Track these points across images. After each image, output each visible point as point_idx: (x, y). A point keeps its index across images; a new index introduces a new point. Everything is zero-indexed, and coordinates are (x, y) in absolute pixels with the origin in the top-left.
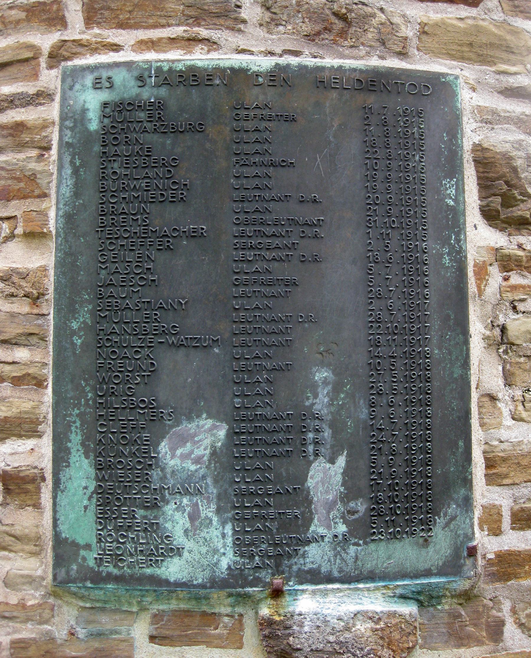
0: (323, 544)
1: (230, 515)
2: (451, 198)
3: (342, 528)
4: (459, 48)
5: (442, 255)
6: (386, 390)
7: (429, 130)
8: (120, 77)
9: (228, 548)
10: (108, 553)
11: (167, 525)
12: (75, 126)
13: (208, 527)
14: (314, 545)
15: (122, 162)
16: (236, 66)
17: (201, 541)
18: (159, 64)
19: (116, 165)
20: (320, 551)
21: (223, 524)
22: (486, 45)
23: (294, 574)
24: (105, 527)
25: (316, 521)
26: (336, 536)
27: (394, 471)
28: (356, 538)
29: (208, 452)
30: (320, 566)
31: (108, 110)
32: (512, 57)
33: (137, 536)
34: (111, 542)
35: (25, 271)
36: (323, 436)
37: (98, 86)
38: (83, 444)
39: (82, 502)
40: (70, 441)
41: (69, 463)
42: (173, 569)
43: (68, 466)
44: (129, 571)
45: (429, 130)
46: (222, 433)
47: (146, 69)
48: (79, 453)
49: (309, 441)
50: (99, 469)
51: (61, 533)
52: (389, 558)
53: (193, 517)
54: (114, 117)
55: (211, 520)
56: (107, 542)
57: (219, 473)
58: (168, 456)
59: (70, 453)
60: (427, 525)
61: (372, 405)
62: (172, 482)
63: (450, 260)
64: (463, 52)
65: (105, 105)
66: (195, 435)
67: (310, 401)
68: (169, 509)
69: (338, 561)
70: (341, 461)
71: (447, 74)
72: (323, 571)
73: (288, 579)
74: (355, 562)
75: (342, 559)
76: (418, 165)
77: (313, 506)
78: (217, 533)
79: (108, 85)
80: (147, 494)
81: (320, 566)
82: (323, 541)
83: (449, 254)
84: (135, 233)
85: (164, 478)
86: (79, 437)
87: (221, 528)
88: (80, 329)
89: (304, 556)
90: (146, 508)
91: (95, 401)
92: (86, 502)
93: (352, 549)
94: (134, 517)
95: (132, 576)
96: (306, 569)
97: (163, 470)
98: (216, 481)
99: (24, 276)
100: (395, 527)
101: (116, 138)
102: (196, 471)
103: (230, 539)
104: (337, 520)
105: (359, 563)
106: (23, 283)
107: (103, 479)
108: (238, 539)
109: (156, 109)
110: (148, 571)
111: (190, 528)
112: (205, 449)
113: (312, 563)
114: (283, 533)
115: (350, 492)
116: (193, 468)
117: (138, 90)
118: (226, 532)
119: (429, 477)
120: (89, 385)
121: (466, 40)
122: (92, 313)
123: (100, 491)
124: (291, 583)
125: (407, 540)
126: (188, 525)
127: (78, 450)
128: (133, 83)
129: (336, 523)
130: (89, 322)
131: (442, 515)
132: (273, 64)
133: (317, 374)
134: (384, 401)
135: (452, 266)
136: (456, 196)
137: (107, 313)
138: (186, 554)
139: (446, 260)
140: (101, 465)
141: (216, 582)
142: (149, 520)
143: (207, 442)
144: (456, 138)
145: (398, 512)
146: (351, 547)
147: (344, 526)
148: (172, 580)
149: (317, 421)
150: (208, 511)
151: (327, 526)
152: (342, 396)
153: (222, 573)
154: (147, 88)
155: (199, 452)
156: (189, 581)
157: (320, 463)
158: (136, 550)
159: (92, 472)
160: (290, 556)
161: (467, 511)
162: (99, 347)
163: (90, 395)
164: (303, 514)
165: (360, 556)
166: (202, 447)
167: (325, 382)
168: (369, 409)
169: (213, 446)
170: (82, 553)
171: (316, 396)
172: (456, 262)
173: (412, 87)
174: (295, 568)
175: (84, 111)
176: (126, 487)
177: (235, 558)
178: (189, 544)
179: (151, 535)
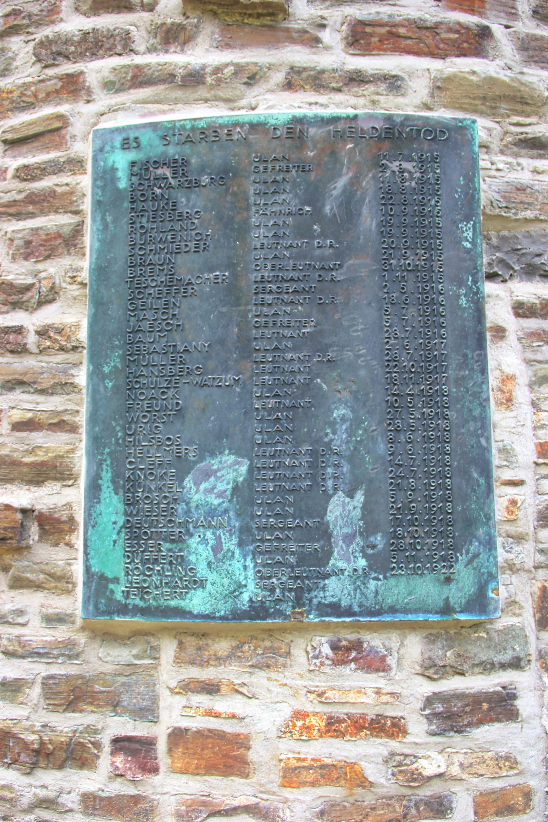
0: (343, 577)
1: (251, 548)
2: (468, 241)
3: (362, 563)
4: (472, 102)
5: (458, 297)
6: (403, 427)
7: (445, 174)
8: (146, 137)
9: (249, 581)
10: (134, 585)
11: (191, 558)
12: (105, 185)
13: (230, 560)
14: (334, 578)
15: (149, 217)
16: (255, 121)
17: (224, 573)
18: (182, 123)
19: (144, 220)
20: (340, 585)
21: (245, 557)
22: (500, 97)
23: (314, 607)
24: (133, 561)
25: (335, 554)
26: (355, 570)
27: (413, 507)
28: (375, 572)
29: (230, 486)
30: (340, 600)
31: (135, 169)
32: (528, 109)
33: (162, 568)
34: (138, 575)
35: (60, 326)
36: (342, 471)
37: (126, 146)
38: (113, 481)
39: (111, 536)
40: (101, 479)
41: (99, 499)
42: (197, 602)
43: (99, 502)
44: (154, 603)
45: (445, 174)
46: (244, 469)
47: (170, 128)
48: (110, 490)
49: (328, 477)
50: (127, 504)
51: (90, 567)
52: (410, 594)
53: (217, 549)
54: (141, 175)
55: (233, 553)
56: (135, 575)
57: (240, 507)
58: (193, 491)
59: (100, 490)
60: (449, 561)
61: (391, 441)
62: (196, 516)
63: (468, 301)
64: (475, 105)
65: (133, 164)
66: (219, 470)
67: (329, 438)
68: (193, 542)
69: (358, 595)
70: (360, 497)
71: (465, 119)
72: (343, 605)
73: (309, 612)
74: (376, 596)
75: (362, 593)
76: (434, 209)
77: (333, 540)
78: (239, 565)
79: (135, 145)
80: (172, 527)
81: (340, 600)
82: (343, 574)
83: (465, 295)
84: (162, 282)
85: (188, 512)
86: (110, 474)
87: (243, 561)
88: (110, 372)
89: (324, 589)
90: (173, 541)
91: (124, 440)
92: (115, 537)
93: (372, 584)
94: (160, 551)
95: (157, 608)
96: (326, 602)
97: (187, 504)
98: (238, 515)
99: (59, 331)
100: (416, 563)
101: (143, 195)
102: (219, 505)
103: (252, 571)
104: (357, 554)
105: (379, 597)
106: (58, 338)
107: (131, 515)
108: (259, 571)
109: (179, 166)
110: (173, 603)
111: (213, 561)
112: (227, 484)
113: (332, 596)
114: (303, 566)
115: (369, 527)
116: (216, 502)
117: (164, 148)
118: (247, 564)
119: (450, 513)
120: (119, 425)
121: (480, 93)
122: (123, 358)
123: (128, 526)
124: (311, 617)
125: (429, 576)
126: (212, 558)
127: (108, 487)
128: (157, 142)
129: (355, 557)
130: (119, 366)
131: (464, 552)
132: (290, 117)
133: (336, 411)
134: (402, 438)
135: (469, 307)
136: (473, 239)
137: (136, 357)
138: (209, 586)
139: (463, 301)
140: (129, 500)
141: (238, 614)
142: (174, 552)
143: (231, 476)
144: (473, 182)
145: (419, 548)
146: (371, 581)
147: (364, 560)
148: (195, 612)
149: (335, 456)
150: (230, 543)
151: (347, 560)
152: (360, 432)
153: (244, 605)
154: (171, 146)
155: (221, 487)
156: (212, 613)
157: (339, 497)
158: (161, 583)
159: (121, 507)
160: (310, 590)
161: (490, 550)
162: (129, 389)
163: (120, 434)
164: (322, 548)
165: (380, 592)
166: (225, 482)
167: (343, 419)
168: (386, 445)
169: (235, 481)
170: (111, 586)
171: (334, 433)
172: (473, 301)
173: (428, 132)
174: (315, 601)
175: (114, 170)
176: (152, 528)
177: (256, 590)
178: (212, 577)
179: (175, 568)
